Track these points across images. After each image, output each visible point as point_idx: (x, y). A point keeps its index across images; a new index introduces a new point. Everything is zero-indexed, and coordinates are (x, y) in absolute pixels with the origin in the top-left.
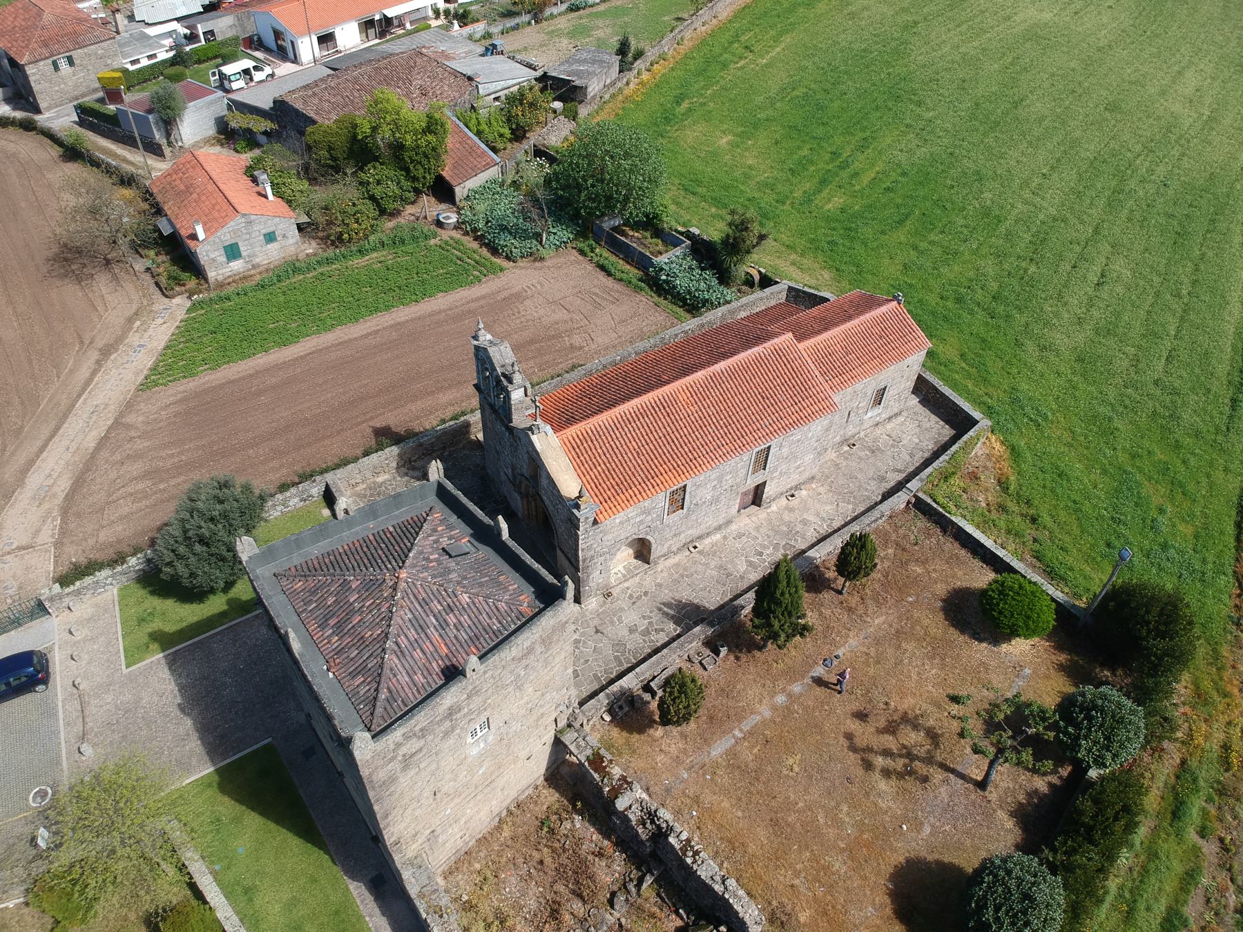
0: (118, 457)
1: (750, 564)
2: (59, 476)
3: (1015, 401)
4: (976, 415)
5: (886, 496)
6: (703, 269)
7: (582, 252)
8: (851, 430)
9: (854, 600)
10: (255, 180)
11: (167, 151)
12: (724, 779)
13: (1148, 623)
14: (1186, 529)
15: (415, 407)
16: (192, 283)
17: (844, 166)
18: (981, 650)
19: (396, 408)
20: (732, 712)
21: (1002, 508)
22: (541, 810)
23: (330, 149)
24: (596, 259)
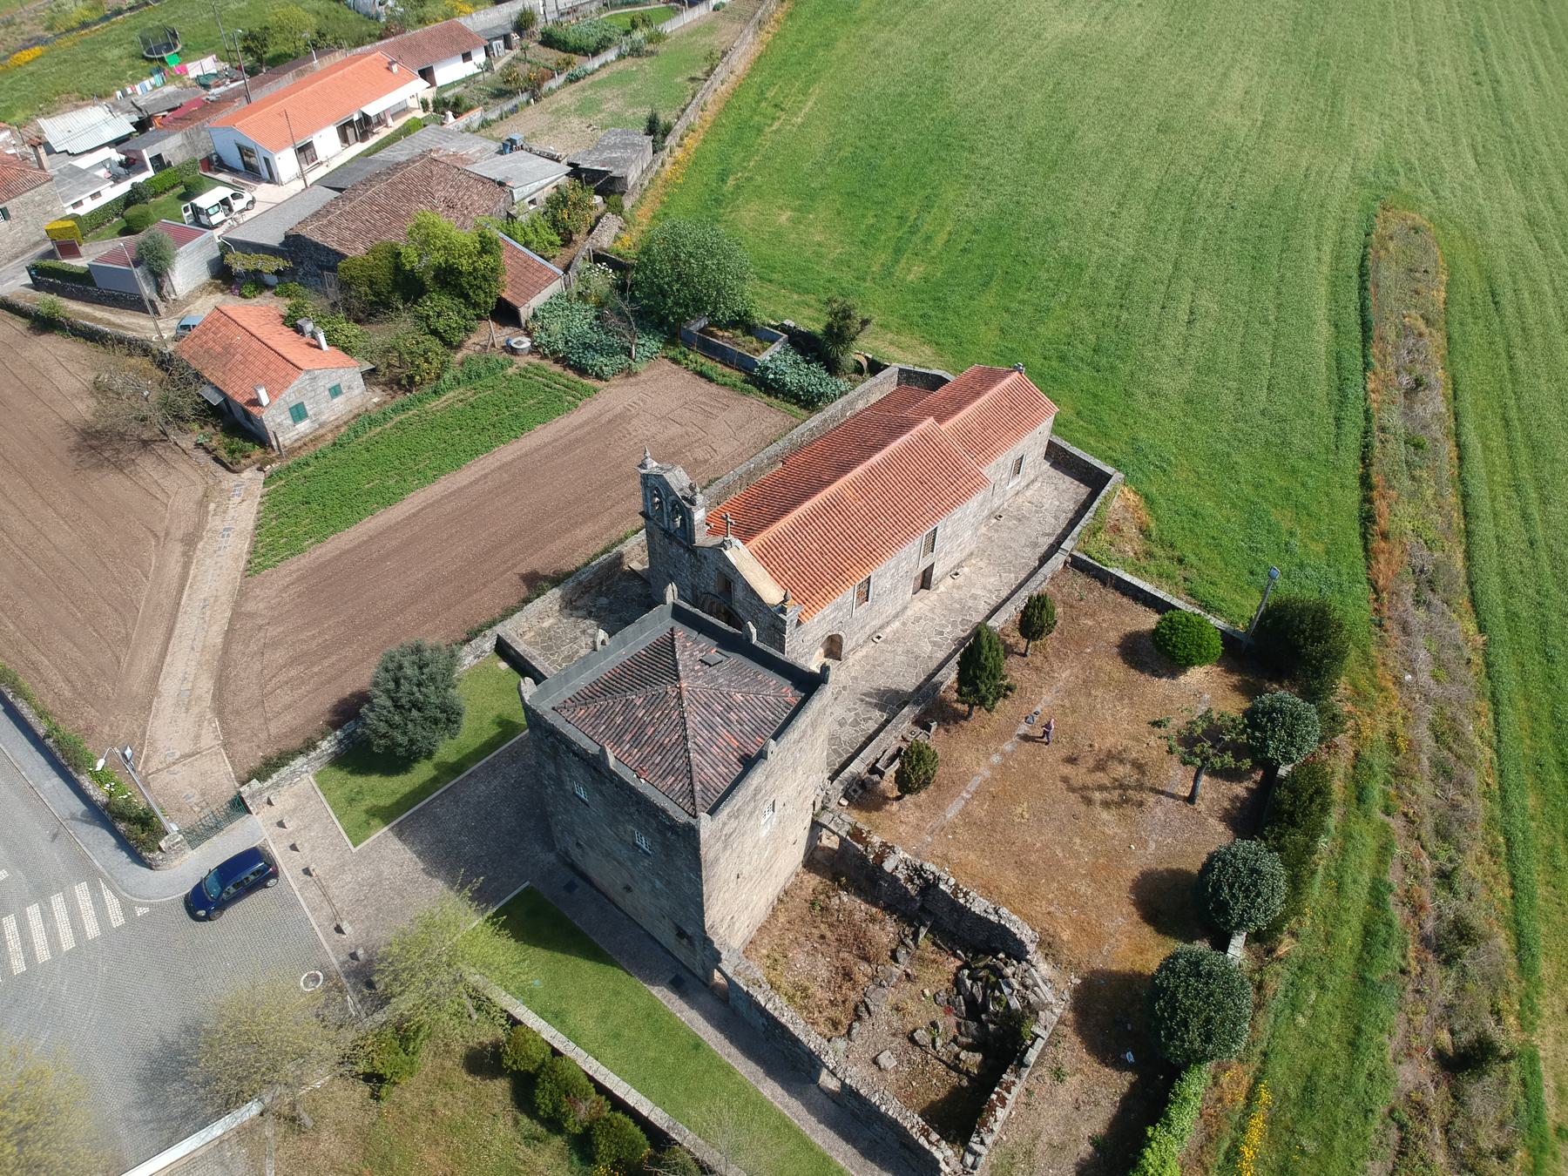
0: (254, 648)
1: (935, 644)
2: (196, 678)
3: (1137, 451)
4: (1109, 470)
5: (1044, 559)
7: (675, 361)
8: (997, 502)
9: (1038, 660)
10: (299, 330)
11: (161, 307)
12: (964, 835)
13: (1303, 632)
14: (1317, 548)
15: (557, 546)
16: (257, 452)
17: (913, 230)
18: (1162, 686)
19: (536, 551)
20: (955, 778)
21: (1149, 555)
22: (807, 893)
23: (371, 284)
24: (692, 366)
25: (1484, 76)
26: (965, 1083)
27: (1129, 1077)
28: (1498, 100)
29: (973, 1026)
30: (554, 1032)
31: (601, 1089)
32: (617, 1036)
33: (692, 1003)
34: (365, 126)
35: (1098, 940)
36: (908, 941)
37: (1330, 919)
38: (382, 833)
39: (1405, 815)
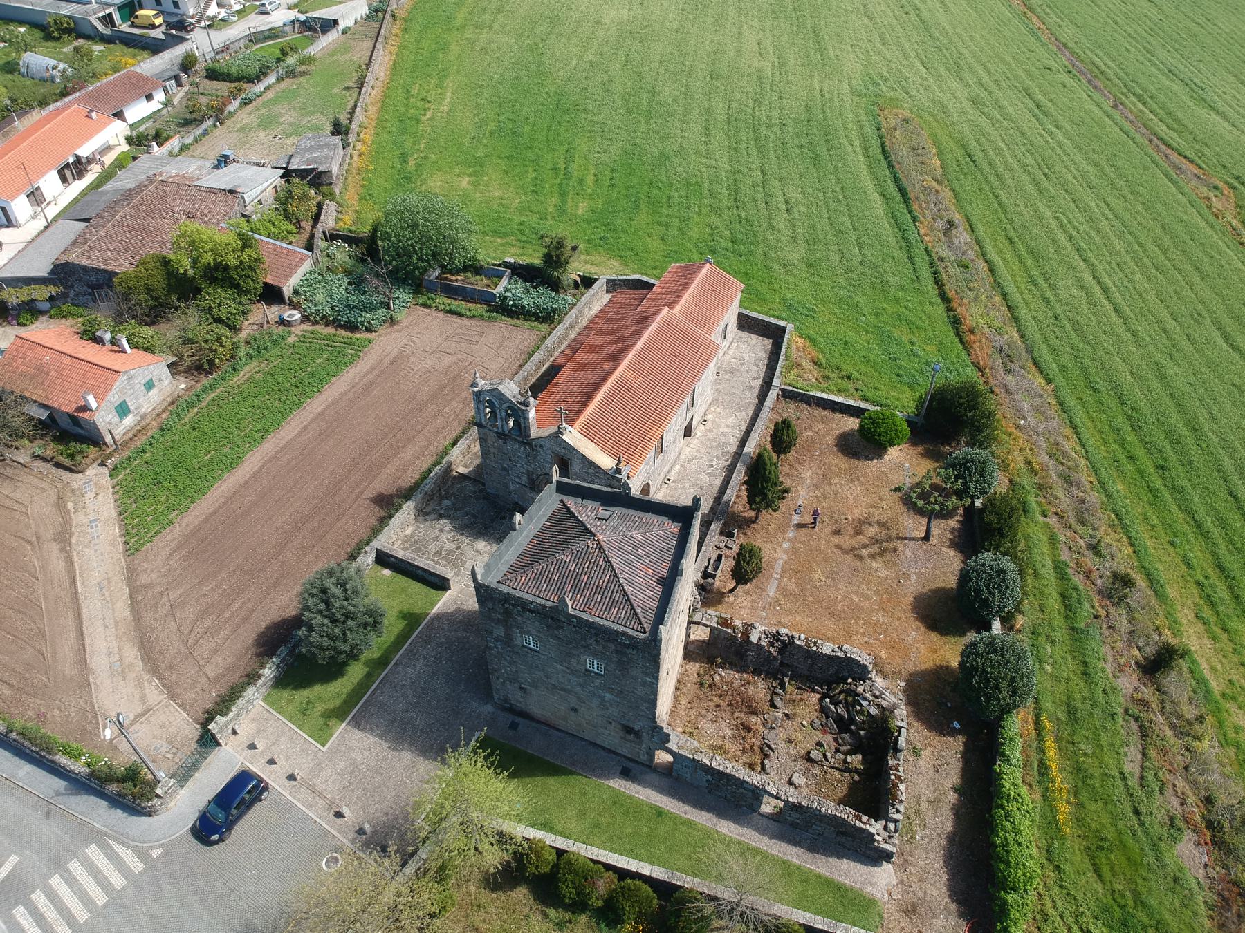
0: (162, 612)
2: (120, 650)
3: (790, 307)
4: (782, 323)
6: (535, 287)
7: (425, 306)
13: (962, 404)
14: (931, 349)
15: (390, 469)
16: (93, 451)
19: (375, 477)
21: (826, 378)
22: (694, 677)
23: (149, 290)
25: (908, 8)
26: (857, 778)
27: (961, 739)
28: (923, 22)
29: (847, 736)
30: (553, 837)
31: (608, 867)
32: (598, 825)
33: (643, 783)
34: (78, 167)
35: (905, 652)
36: (778, 691)
37: (1038, 596)
38: (341, 729)
39: (1056, 514)
